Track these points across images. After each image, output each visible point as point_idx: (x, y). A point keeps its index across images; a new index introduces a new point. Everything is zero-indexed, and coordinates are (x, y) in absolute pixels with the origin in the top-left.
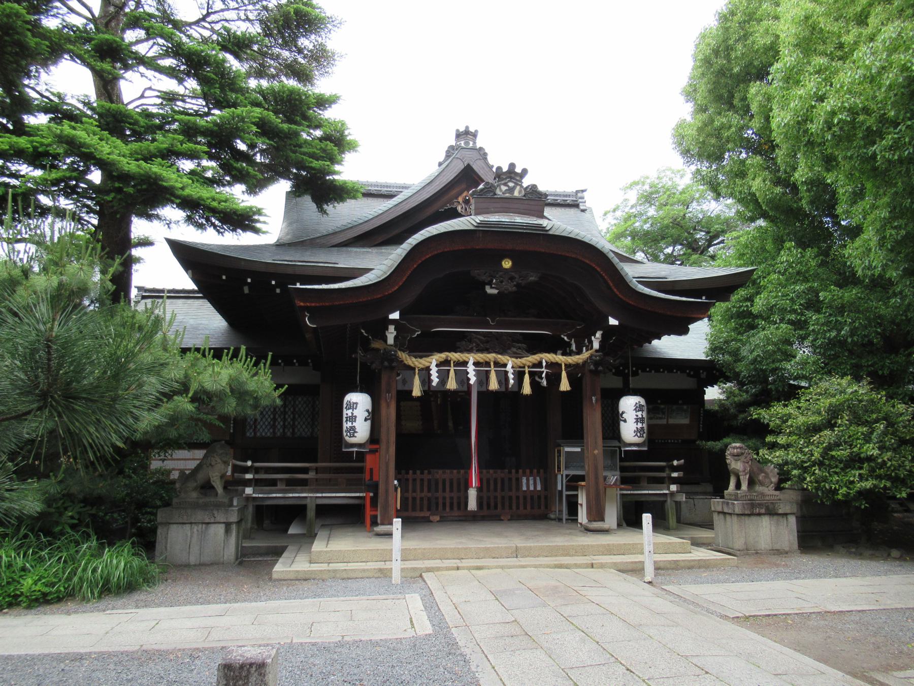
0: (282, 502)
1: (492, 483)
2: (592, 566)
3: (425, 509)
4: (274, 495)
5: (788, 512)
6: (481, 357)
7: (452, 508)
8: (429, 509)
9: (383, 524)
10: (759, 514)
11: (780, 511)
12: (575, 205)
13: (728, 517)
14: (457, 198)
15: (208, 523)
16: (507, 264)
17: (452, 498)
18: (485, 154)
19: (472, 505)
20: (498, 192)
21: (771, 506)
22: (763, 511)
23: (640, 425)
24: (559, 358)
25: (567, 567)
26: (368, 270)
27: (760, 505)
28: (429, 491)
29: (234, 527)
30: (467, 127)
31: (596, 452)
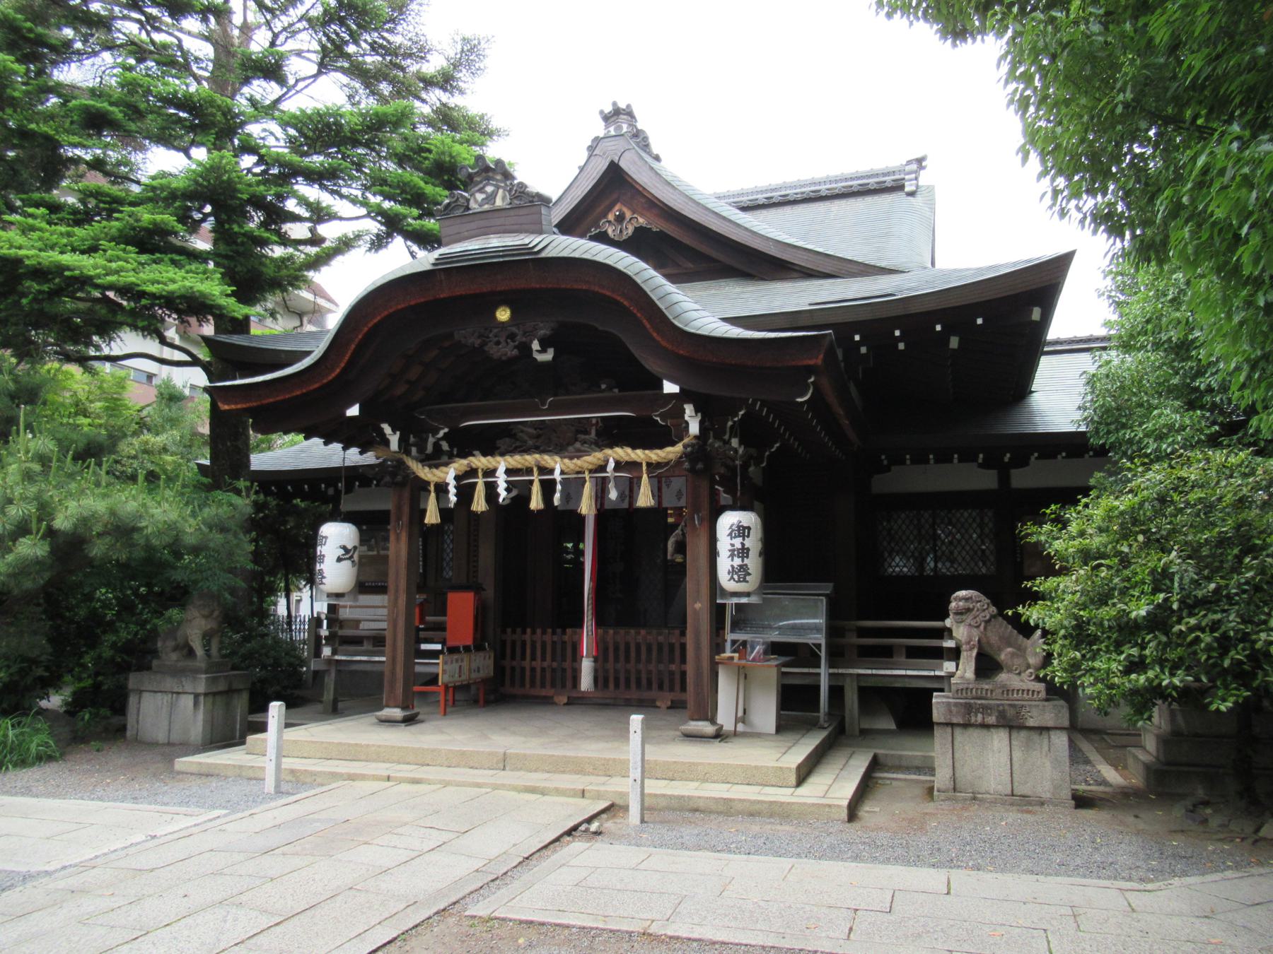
0: (368, 668)
1: (644, 649)
2: (583, 793)
3: (548, 684)
4: (358, 658)
5: (1050, 724)
6: (516, 461)
7: (617, 686)
8: (553, 685)
9: (388, 706)
10: (984, 726)
11: (1031, 723)
12: (898, 187)
13: (958, 731)
14: (605, 216)
15: (178, 693)
16: (503, 315)
17: (616, 671)
18: (645, 139)
19: (586, 682)
20: (473, 205)
21: (1010, 713)
22: (992, 720)
23: (737, 561)
24: (639, 455)
25: (543, 792)
26: (308, 353)
27: (985, 709)
28: (553, 660)
29: (202, 698)
30: (614, 104)
31: (698, 606)
